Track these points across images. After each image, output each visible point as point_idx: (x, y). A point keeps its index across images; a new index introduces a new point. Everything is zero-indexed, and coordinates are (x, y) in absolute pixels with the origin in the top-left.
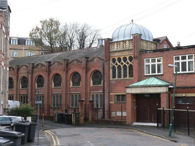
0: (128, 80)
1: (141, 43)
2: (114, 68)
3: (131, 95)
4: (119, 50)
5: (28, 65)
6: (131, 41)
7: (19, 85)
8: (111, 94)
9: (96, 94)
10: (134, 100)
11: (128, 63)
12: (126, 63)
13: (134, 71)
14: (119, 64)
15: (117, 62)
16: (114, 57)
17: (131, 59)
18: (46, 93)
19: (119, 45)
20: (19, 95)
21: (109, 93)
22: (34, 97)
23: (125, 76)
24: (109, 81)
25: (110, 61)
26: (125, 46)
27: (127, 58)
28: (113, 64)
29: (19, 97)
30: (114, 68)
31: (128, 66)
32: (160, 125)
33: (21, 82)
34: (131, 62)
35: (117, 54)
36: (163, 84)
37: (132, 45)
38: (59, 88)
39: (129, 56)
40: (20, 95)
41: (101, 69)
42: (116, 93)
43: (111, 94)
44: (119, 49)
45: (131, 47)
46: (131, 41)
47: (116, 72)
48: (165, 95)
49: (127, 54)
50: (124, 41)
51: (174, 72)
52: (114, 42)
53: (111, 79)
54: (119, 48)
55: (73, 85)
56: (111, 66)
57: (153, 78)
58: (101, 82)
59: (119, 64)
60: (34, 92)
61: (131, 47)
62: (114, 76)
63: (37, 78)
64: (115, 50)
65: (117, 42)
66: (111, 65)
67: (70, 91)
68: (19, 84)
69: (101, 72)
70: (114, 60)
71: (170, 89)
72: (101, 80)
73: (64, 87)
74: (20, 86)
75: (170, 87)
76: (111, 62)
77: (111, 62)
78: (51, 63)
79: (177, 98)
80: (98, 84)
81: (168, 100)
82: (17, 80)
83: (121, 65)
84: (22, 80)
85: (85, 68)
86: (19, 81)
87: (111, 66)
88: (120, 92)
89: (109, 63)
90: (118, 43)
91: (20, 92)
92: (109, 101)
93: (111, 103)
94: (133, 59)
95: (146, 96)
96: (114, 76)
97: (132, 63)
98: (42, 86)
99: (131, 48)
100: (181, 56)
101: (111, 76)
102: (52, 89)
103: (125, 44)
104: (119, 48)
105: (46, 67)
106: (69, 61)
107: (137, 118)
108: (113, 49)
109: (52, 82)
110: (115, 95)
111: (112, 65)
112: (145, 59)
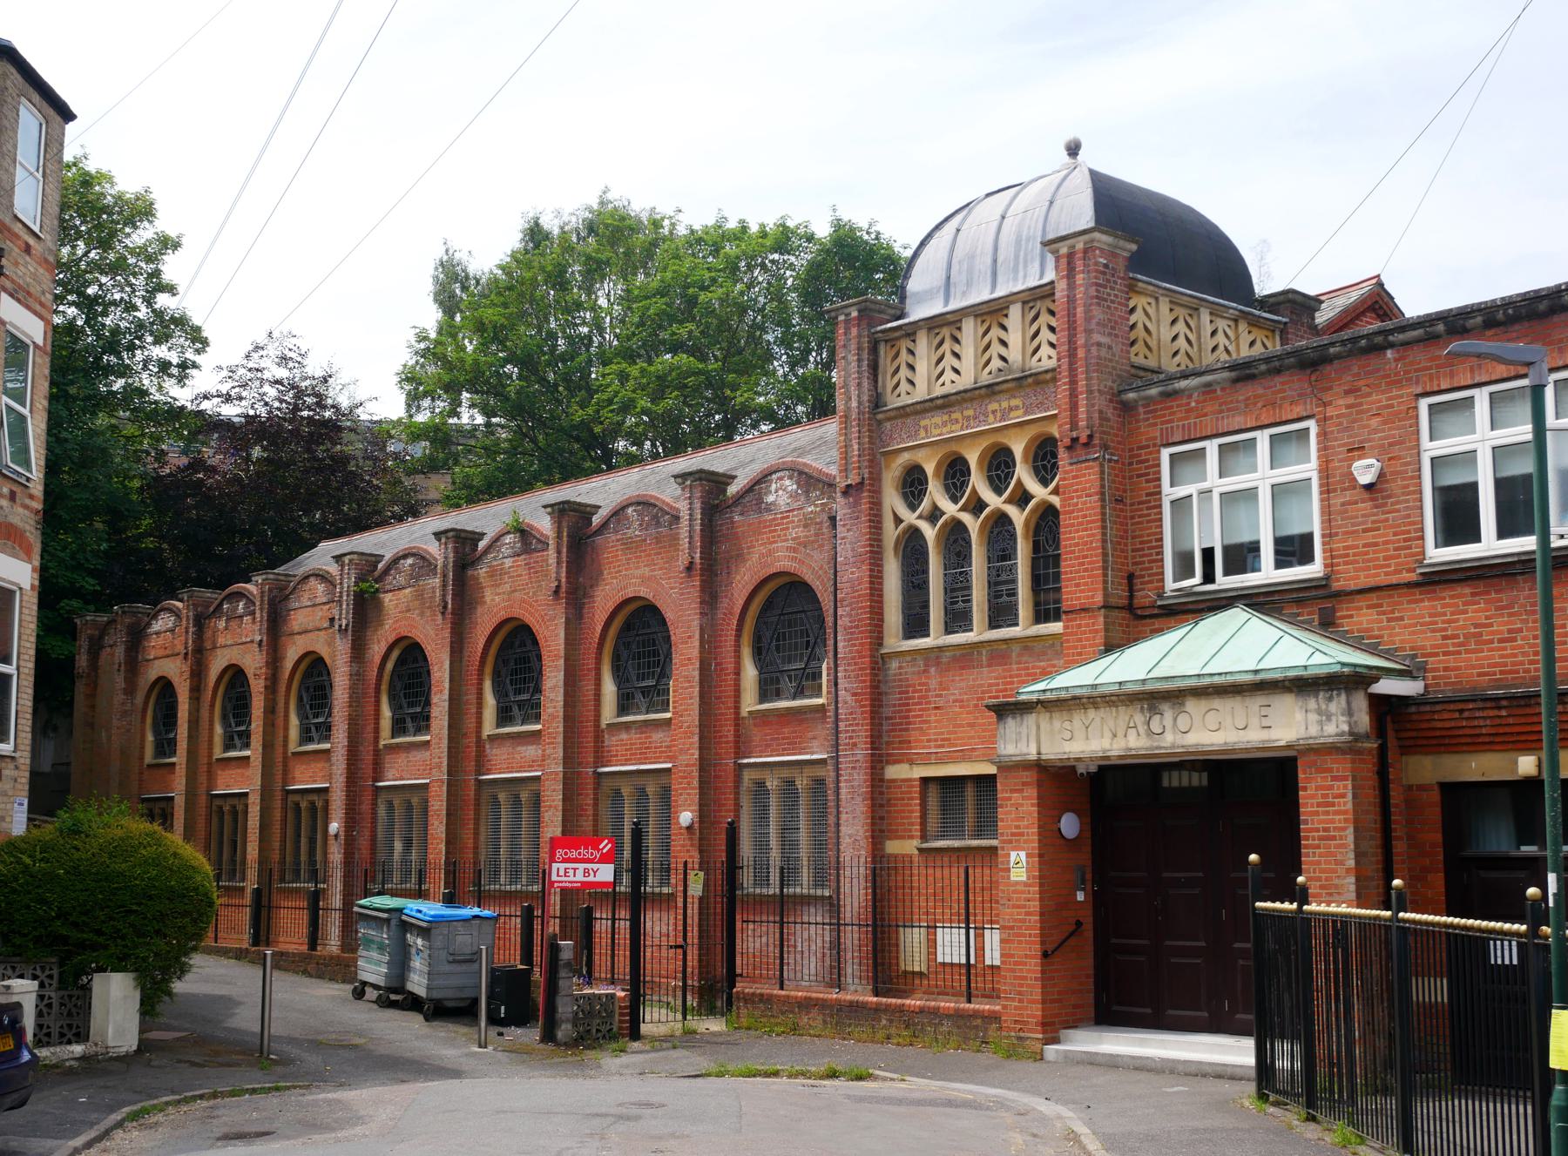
0: (1026, 643)
1: (1138, 317)
2: (912, 545)
3: (1029, 776)
4: (949, 389)
5: (333, 569)
6: (1041, 306)
7: (280, 721)
8: (894, 772)
9: (786, 773)
10: (1069, 825)
11: (1022, 498)
12: (1006, 502)
13: (1067, 566)
14: (993, 501)
15: (978, 483)
16: (954, 447)
17: (1044, 459)
18: (691, 755)
19: (947, 346)
20: (278, 796)
21: (877, 761)
22: (366, 807)
23: (1001, 613)
24: (878, 662)
25: (876, 492)
26: (996, 348)
27: (1018, 449)
28: (910, 517)
29: (285, 809)
30: (912, 545)
31: (938, 537)
32: (1286, 1059)
33: (300, 699)
34: (1045, 482)
35: (937, 428)
36: (1318, 659)
37: (1053, 338)
38: (519, 735)
39: (1032, 431)
40: (291, 798)
41: (813, 571)
42: (926, 760)
43: (894, 772)
44: (950, 384)
45: (1045, 350)
46: (1048, 303)
47: (926, 582)
48: (1341, 766)
49: (1017, 417)
50: (991, 313)
51: (1423, 553)
52: (911, 332)
53: (894, 641)
54: (949, 375)
55: (623, 709)
56: (891, 533)
57: (1238, 615)
58: (817, 675)
59: (993, 501)
60: (370, 772)
61: (1045, 350)
62: (916, 624)
63: (390, 666)
64: (920, 393)
65: (934, 324)
66: (888, 523)
67: (600, 760)
68: (281, 704)
69: (816, 585)
70: (913, 484)
71: (1384, 707)
72: (820, 660)
73: (692, 716)
74: (286, 729)
75: (1386, 687)
76: (893, 500)
77: (893, 500)
78: (482, 545)
79: (1458, 795)
80: (799, 693)
81: (1372, 819)
82: (196, 690)
83: (966, 518)
84: (302, 683)
85: (123, 668)
86: (282, 688)
87: (891, 533)
88: (964, 756)
89: (876, 505)
90: (946, 332)
91: (286, 772)
92: (880, 828)
93: (893, 847)
94: (1062, 454)
95: (1172, 780)
96: (916, 624)
97: (1056, 492)
98: (657, 696)
99: (1048, 364)
100: (1487, 390)
101: (893, 616)
102: (480, 743)
103: (995, 332)
104: (949, 375)
105: (445, 576)
106: (596, 520)
107: (875, 980)
108: (904, 386)
109: (287, 716)
110: (925, 781)
111: (898, 520)
112: (1165, 454)
